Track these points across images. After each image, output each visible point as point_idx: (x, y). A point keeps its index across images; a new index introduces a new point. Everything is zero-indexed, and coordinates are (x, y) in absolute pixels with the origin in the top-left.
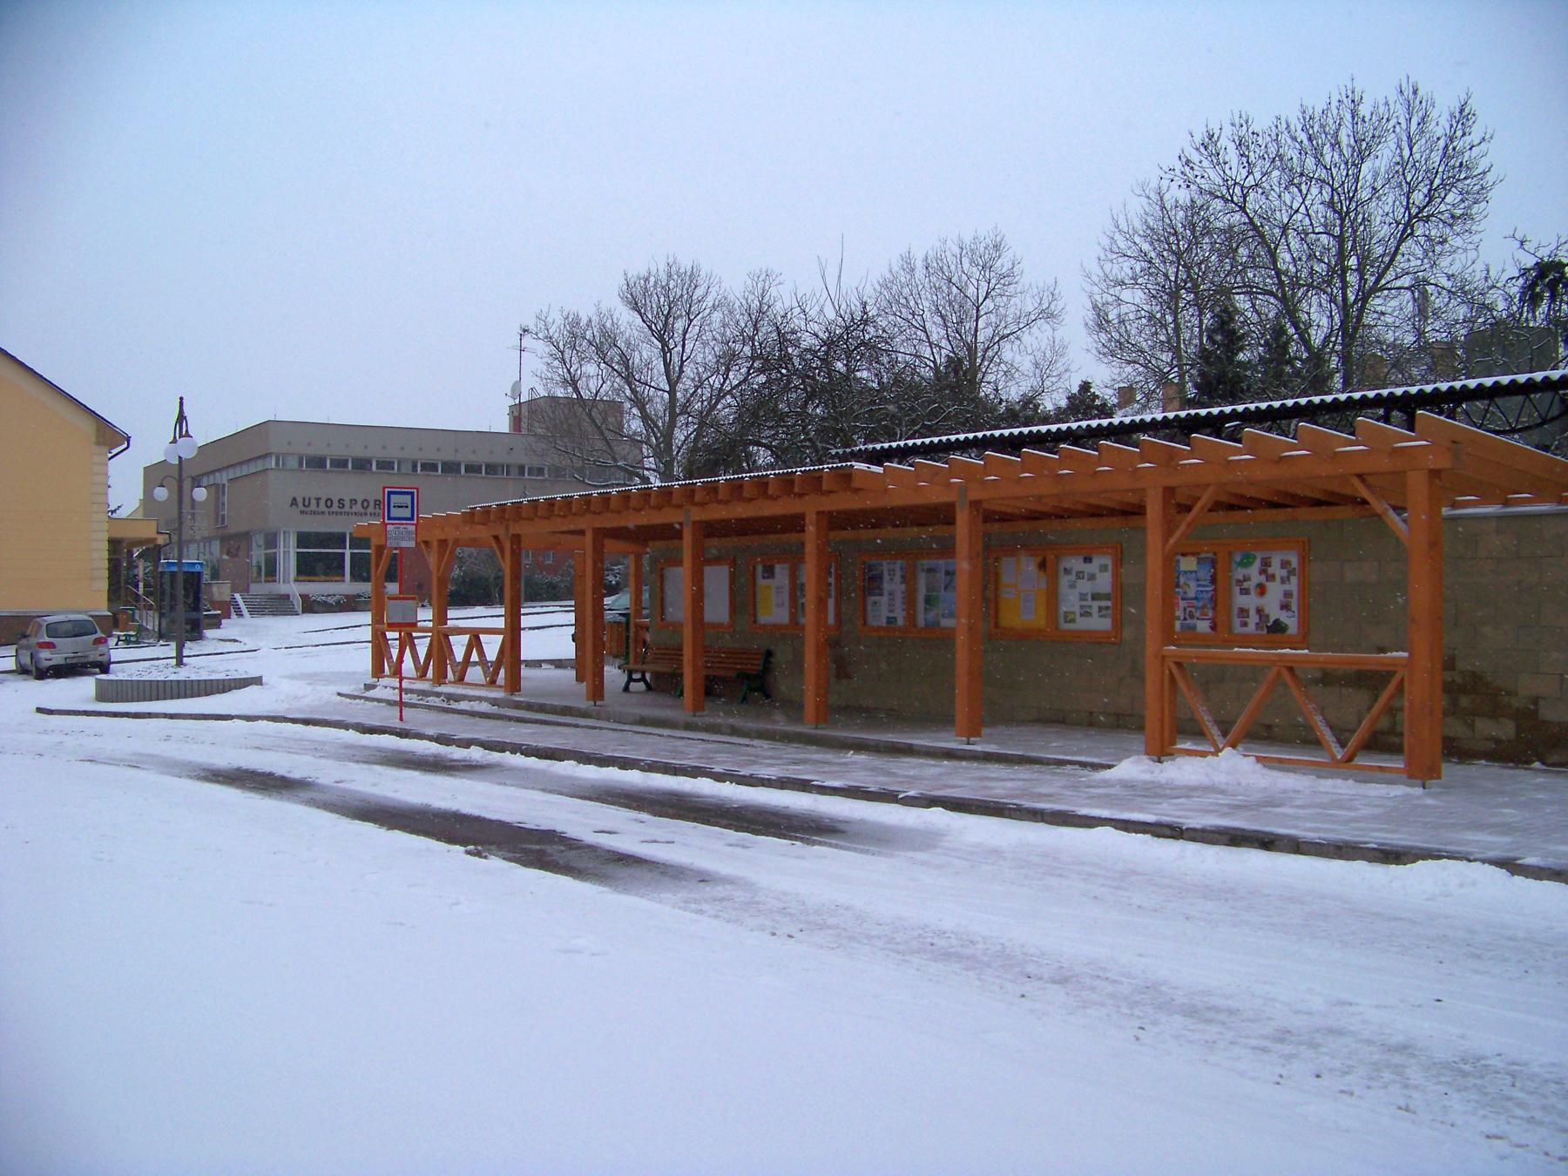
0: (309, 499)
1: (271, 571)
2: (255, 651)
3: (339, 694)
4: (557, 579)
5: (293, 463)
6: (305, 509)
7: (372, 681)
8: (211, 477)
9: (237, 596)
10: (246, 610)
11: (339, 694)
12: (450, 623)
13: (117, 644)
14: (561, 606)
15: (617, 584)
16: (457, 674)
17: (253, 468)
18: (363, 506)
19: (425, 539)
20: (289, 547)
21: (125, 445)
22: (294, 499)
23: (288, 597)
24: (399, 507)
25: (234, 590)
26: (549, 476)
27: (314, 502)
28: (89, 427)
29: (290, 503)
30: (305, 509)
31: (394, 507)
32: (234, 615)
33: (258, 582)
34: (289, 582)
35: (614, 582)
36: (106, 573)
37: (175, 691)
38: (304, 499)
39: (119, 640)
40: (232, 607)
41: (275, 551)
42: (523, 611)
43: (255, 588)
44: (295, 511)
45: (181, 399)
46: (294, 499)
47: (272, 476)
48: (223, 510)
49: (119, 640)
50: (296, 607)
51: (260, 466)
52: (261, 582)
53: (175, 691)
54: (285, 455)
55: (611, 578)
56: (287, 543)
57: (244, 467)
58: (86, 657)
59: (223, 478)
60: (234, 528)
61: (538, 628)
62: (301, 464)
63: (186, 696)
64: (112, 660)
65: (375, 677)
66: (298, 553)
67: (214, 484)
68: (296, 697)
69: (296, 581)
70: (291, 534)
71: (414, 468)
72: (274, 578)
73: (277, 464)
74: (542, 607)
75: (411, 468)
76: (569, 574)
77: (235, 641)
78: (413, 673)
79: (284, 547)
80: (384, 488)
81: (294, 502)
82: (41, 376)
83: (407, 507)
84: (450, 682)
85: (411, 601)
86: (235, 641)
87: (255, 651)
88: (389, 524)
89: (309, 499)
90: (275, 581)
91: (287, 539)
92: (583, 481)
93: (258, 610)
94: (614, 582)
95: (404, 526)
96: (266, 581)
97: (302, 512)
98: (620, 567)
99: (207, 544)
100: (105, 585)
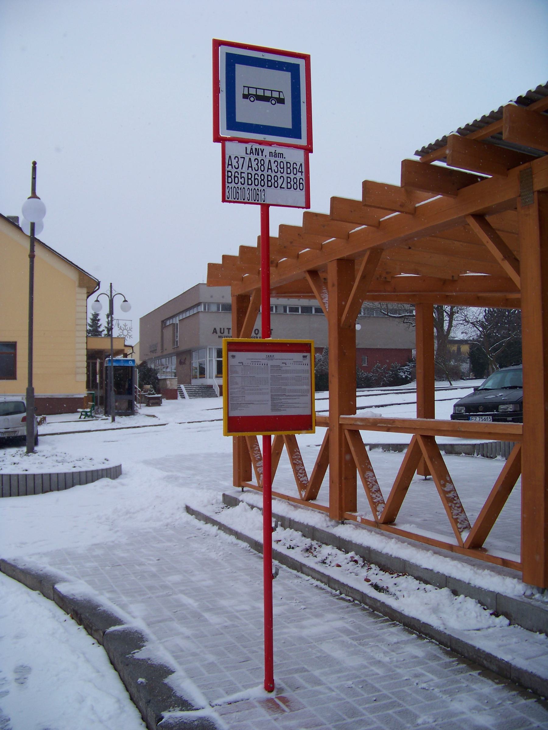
0: (224, 329)
1: (202, 372)
2: (165, 425)
3: (188, 510)
4: (371, 374)
5: (214, 308)
6: (221, 335)
7: (232, 491)
8: (171, 320)
9: (182, 386)
10: (187, 394)
11: (188, 510)
12: (359, 413)
13: (80, 418)
14: (381, 390)
15: (405, 377)
16: (380, 508)
17: (192, 312)
18: (255, 333)
19: (311, 267)
20: (212, 358)
21: (98, 287)
22: (215, 329)
23: (211, 387)
24: (259, 98)
25: (180, 382)
26: (364, 314)
27: (226, 331)
28: (73, 276)
29: (212, 331)
30: (221, 335)
31: (245, 97)
32: (179, 397)
33: (196, 378)
34: (212, 378)
35: (404, 377)
36: (85, 370)
37: (22, 488)
38: (221, 329)
39: (82, 415)
40: (178, 392)
41: (204, 360)
42: (358, 394)
43: (195, 382)
44: (216, 336)
45: (35, 163)
46: (215, 329)
47: (201, 315)
48: (177, 338)
49: (82, 415)
50: (216, 393)
51: (195, 311)
52: (197, 378)
53: (22, 488)
54: (209, 304)
55: (402, 374)
56: (211, 355)
57: (188, 313)
58: (15, 432)
59: (176, 320)
60: (183, 347)
61: (382, 406)
62: (218, 309)
63: (26, 494)
64: (39, 433)
65: (239, 486)
66: (217, 360)
67: (172, 323)
68: (128, 512)
69: (217, 377)
70: (213, 350)
71: (285, 311)
72: (204, 376)
73: (205, 309)
74: (368, 391)
75: (283, 311)
76: (377, 371)
77: (154, 416)
78: (294, 491)
79: (209, 357)
80: (217, 44)
81: (215, 331)
82: (44, 244)
83: (281, 101)
84: (365, 522)
85: (297, 356)
86: (154, 416)
87: (165, 425)
88: (231, 140)
89: (224, 329)
90: (204, 377)
91: (211, 352)
92: (387, 315)
93: (194, 394)
94: (404, 377)
95: (272, 149)
96: (200, 378)
97: (219, 337)
98: (407, 367)
99: (170, 358)
100: (84, 378)
